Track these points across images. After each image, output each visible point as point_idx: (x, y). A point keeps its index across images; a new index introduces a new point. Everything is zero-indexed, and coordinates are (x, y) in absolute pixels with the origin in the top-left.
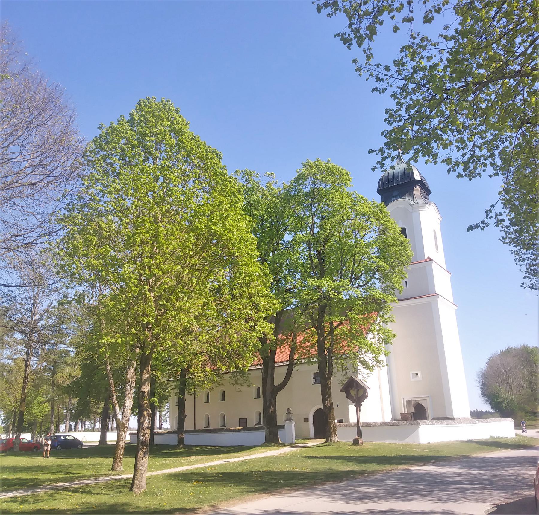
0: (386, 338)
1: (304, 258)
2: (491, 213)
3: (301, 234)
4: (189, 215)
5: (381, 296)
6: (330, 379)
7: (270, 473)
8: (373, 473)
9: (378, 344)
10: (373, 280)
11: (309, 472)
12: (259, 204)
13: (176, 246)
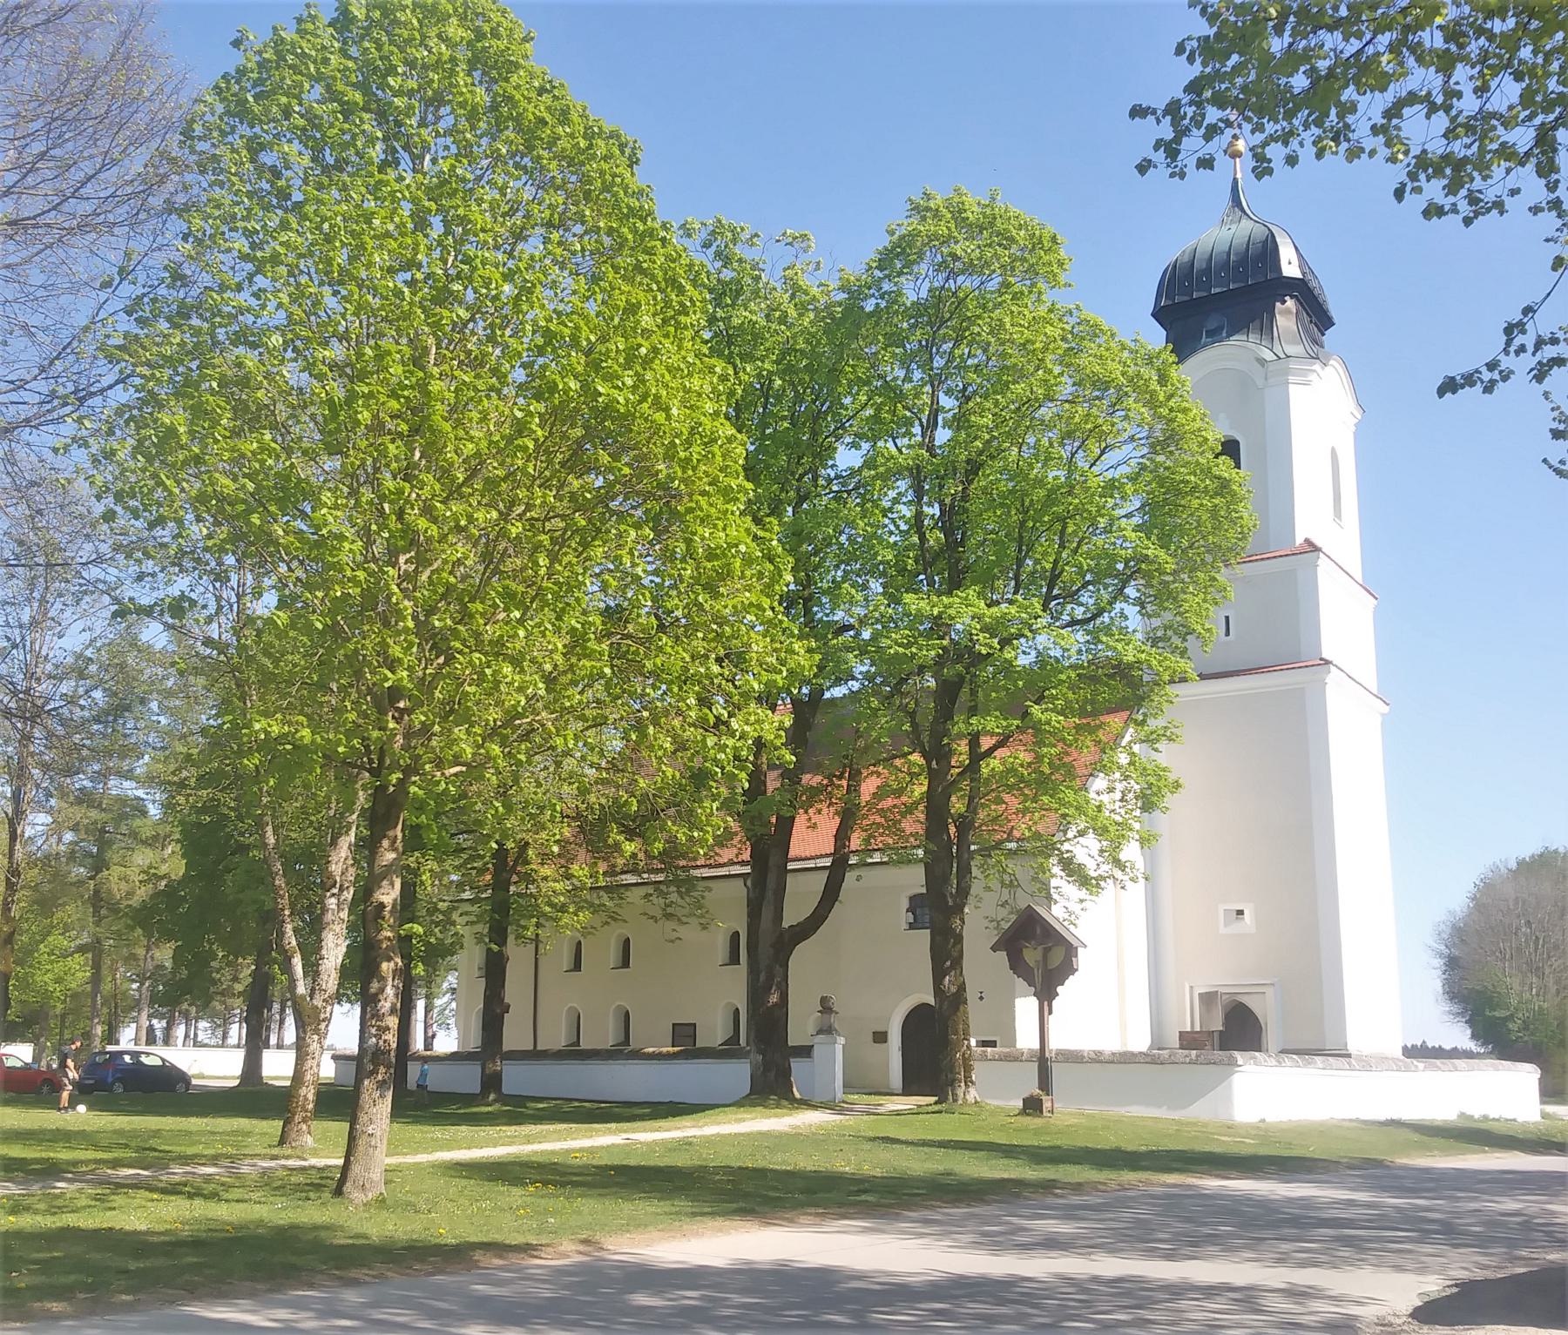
0: (1149, 792)
1: (897, 527)
2: (1524, 332)
3: (890, 445)
4: (525, 346)
5: (1143, 656)
6: (962, 912)
7: (761, 1173)
8: (1078, 1188)
9: (1123, 812)
10: (1118, 606)
11: (882, 1178)
12: (757, 337)
13: (484, 444)
